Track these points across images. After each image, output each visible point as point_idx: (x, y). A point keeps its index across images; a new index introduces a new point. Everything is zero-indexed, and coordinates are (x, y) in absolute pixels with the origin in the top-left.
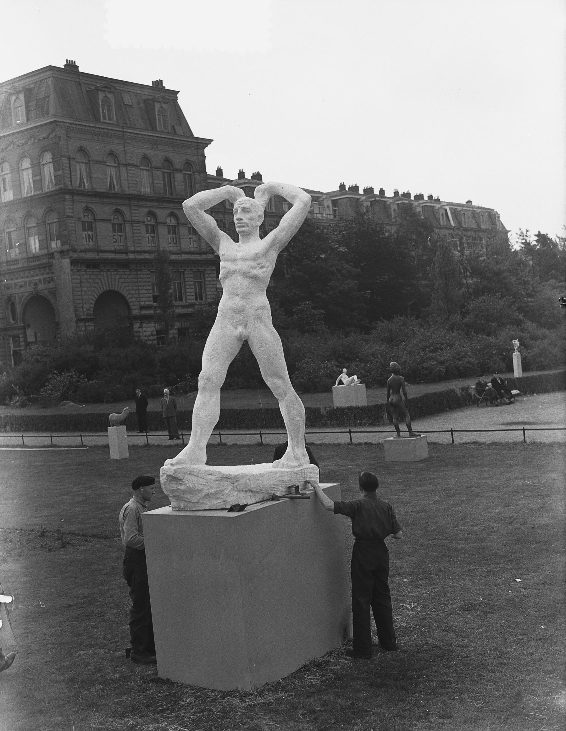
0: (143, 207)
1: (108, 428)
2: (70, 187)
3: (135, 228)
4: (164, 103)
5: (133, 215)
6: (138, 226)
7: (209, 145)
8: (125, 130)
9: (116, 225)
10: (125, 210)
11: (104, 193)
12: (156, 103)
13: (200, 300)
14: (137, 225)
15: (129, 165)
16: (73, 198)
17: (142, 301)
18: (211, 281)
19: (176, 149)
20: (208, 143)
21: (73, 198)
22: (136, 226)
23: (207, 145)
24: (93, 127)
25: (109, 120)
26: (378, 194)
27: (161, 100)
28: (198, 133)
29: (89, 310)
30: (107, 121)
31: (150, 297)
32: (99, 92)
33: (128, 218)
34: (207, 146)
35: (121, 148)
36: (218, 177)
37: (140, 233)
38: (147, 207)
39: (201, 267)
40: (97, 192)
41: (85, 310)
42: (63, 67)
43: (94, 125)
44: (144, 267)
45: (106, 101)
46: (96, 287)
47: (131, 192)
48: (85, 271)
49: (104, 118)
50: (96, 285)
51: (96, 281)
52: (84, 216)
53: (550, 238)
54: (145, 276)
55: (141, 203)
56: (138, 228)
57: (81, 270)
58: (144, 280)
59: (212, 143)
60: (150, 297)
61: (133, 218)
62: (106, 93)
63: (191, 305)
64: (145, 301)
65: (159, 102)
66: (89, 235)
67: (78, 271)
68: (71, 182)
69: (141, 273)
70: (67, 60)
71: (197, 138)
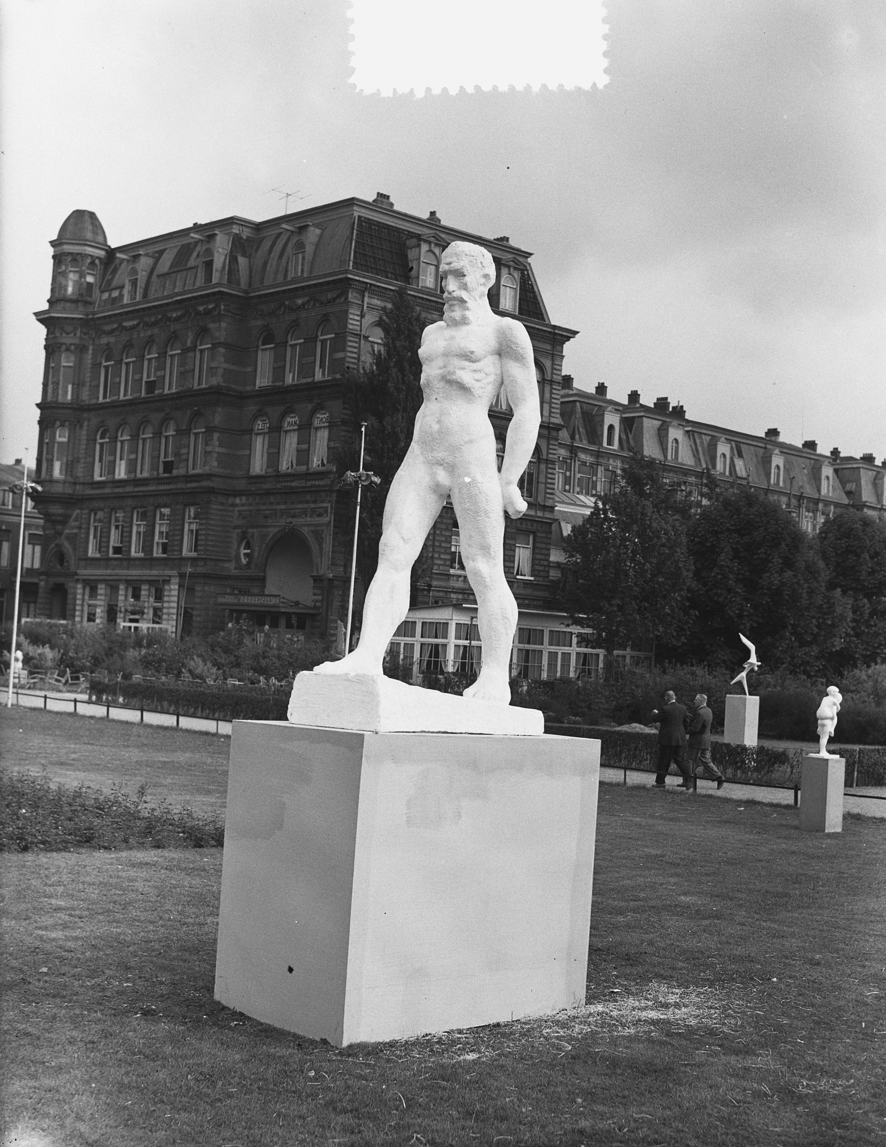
3: (356, 350)
4: (436, 245)
5: (356, 345)
7: (571, 339)
12: (422, 243)
18: (543, 549)
20: (569, 335)
22: (354, 314)
23: (568, 338)
26: (880, 465)
27: (432, 239)
32: (502, 268)
34: (569, 340)
36: (597, 396)
42: (652, 406)
59: (577, 336)
61: (357, 340)
62: (433, 245)
65: (430, 243)
71: (555, 327)
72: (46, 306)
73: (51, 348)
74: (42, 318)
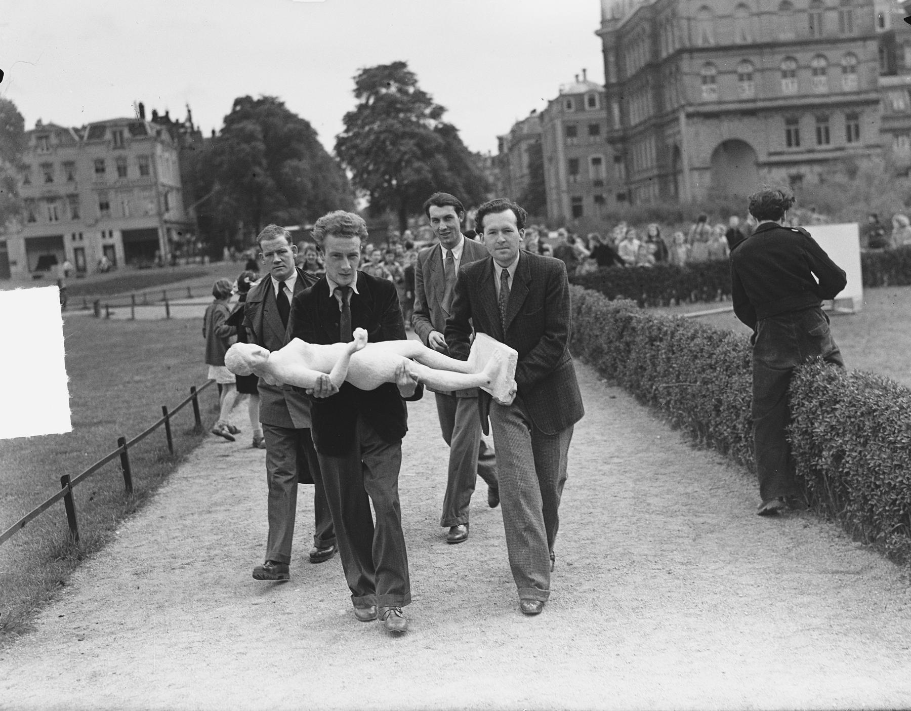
28: (598, 42)
73: (605, 51)
74: (598, 34)
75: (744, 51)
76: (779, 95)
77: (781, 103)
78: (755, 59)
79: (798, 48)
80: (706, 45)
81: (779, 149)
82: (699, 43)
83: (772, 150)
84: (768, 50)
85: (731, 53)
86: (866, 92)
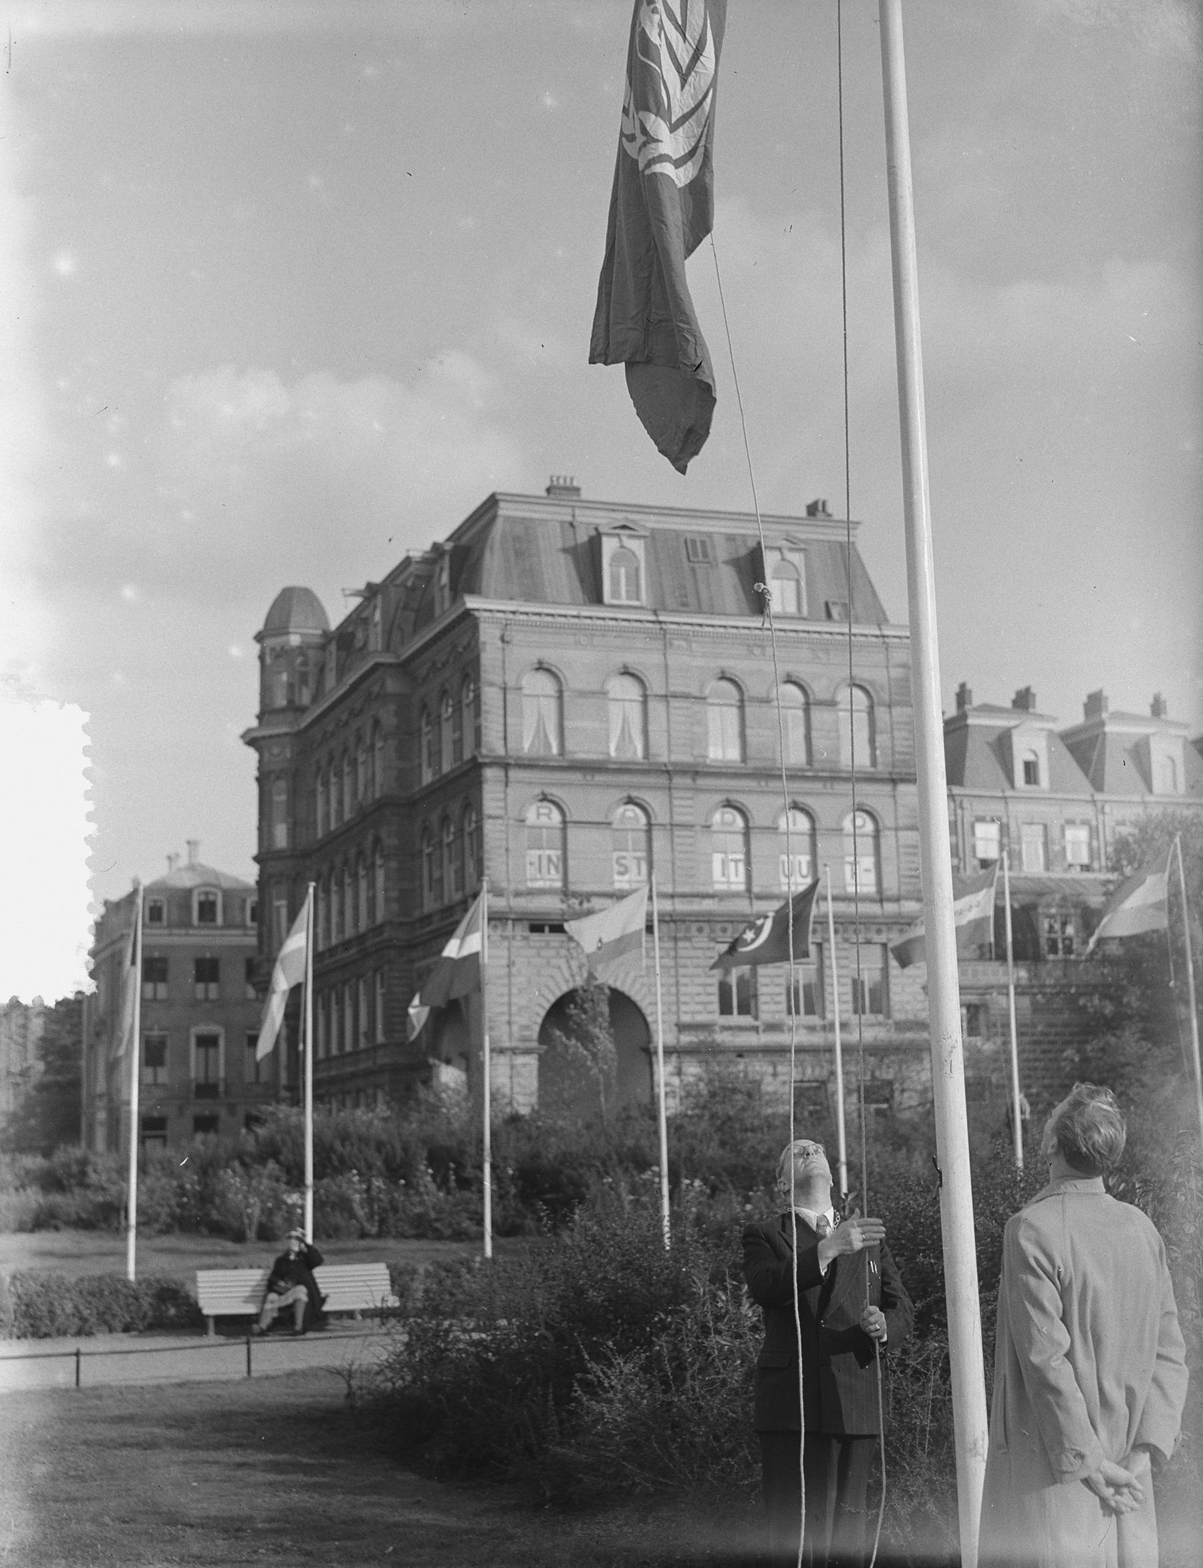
0: (708, 791)
1: (852, 1354)
2: (501, 752)
6: (690, 837)
8: (661, 618)
9: (544, 843)
10: (655, 800)
11: (598, 761)
13: (740, 1013)
14: (689, 833)
15: (676, 697)
16: (506, 776)
17: (685, 1013)
19: (821, 654)
21: (506, 776)
24: (574, 617)
25: (628, 598)
28: (251, 757)
29: (527, 1027)
30: (624, 601)
31: (710, 1003)
33: (661, 816)
35: (657, 658)
37: (692, 852)
38: (717, 791)
39: (879, 932)
40: (577, 761)
41: (515, 1028)
43: (574, 613)
44: (700, 930)
45: (624, 555)
46: (552, 977)
47: (674, 758)
48: (525, 938)
49: (615, 593)
50: (555, 972)
51: (554, 962)
52: (539, 815)
53: (71, 996)
54: (700, 953)
55: (701, 782)
56: (689, 841)
57: (514, 938)
58: (695, 961)
60: (710, 1003)
63: (772, 1027)
64: (693, 1013)
66: (550, 859)
67: (504, 938)
68: (505, 739)
69: (687, 944)
70: (551, 478)
72: (254, 723)
73: (263, 780)
74: (251, 740)
75: (626, 779)
76: (702, 889)
77: (708, 905)
78: (655, 800)
79: (751, 784)
80: (628, 756)
81: (701, 1018)
82: (526, 745)
83: (686, 1019)
84: (687, 781)
85: (600, 778)
86: (897, 899)
